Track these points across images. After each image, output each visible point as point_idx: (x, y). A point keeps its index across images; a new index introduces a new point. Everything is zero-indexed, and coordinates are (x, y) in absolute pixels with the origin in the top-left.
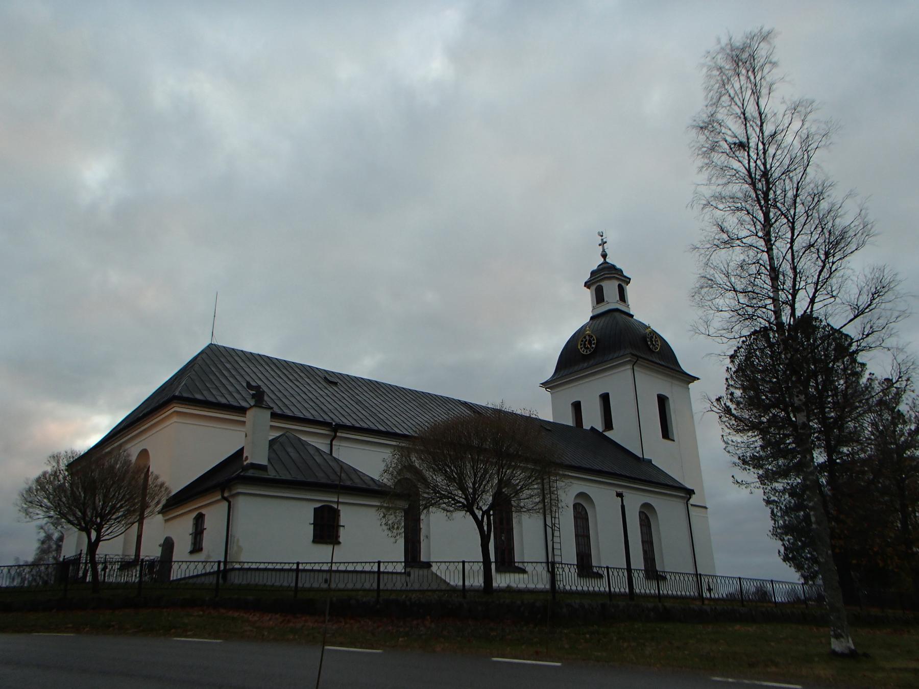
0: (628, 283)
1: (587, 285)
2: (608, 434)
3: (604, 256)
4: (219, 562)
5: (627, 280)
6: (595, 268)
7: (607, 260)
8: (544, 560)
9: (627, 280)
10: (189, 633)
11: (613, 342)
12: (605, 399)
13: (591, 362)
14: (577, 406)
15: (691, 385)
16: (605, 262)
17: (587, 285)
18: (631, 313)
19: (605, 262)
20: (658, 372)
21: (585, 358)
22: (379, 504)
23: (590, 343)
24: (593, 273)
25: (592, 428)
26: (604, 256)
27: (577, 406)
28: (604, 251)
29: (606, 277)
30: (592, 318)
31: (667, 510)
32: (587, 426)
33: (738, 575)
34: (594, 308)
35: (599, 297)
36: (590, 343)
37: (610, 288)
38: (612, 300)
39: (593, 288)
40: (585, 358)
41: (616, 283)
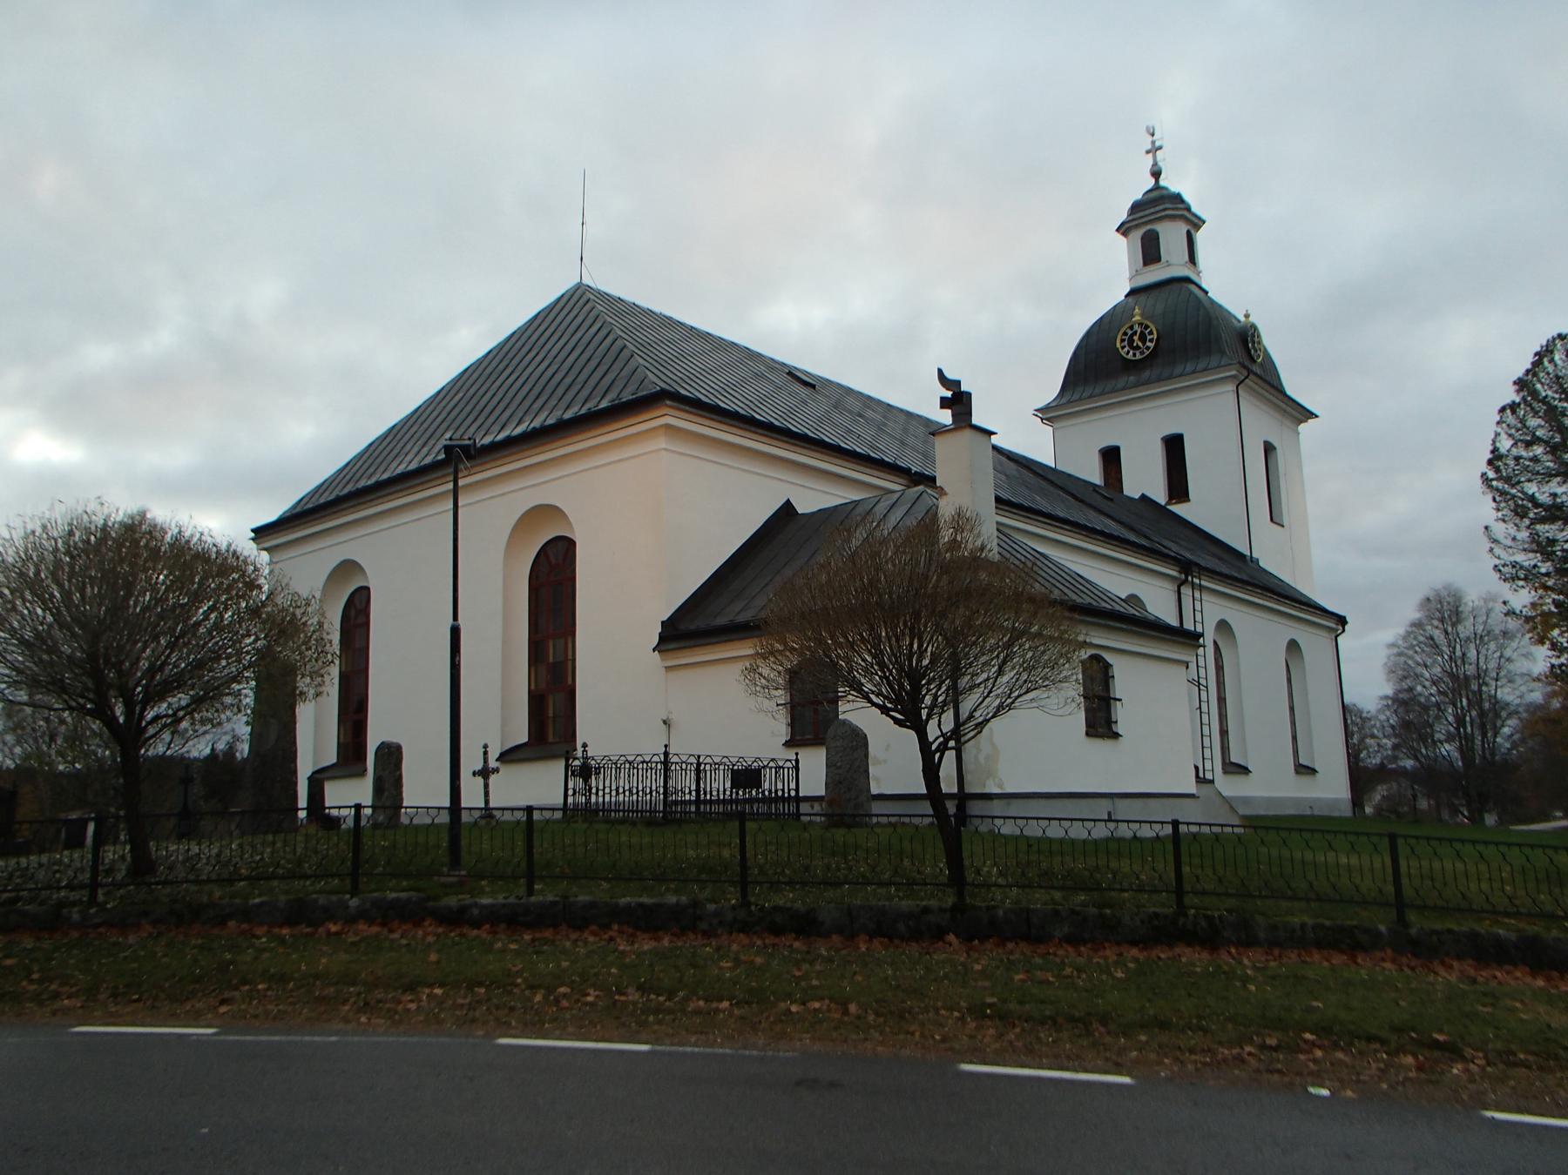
1: (1124, 229)
2: (1177, 509)
3: (1156, 174)
4: (358, 807)
5: (1196, 223)
6: (1139, 196)
7: (1162, 183)
9: (1196, 223)
11: (1166, 338)
12: (1174, 447)
13: (1147, 374)
14: (1111, 457)
15: (1302, 427)
16: (1157, 187)
17: (1124, 229)
19: (1157, 187)
21: (1129, 366)
22: (751, 652)
23: (1143, 338)
24: (1136, 207)
25: (1143, 497)
26: (1156, 174)
27: (1111, 457)
28: (1155, 164)
29: (1157, 215)
30: (1133, 293)
31: (1313, 642)
32: (1132, 489)
33: (523, 803)
34: (1135, 275)
35: (1151, 252)
36: (1143, 338)
37: (1171, 236)
38: (1173, 264)
39: (1137, 235)
40: (1129, 366)
41: (1183, 228)
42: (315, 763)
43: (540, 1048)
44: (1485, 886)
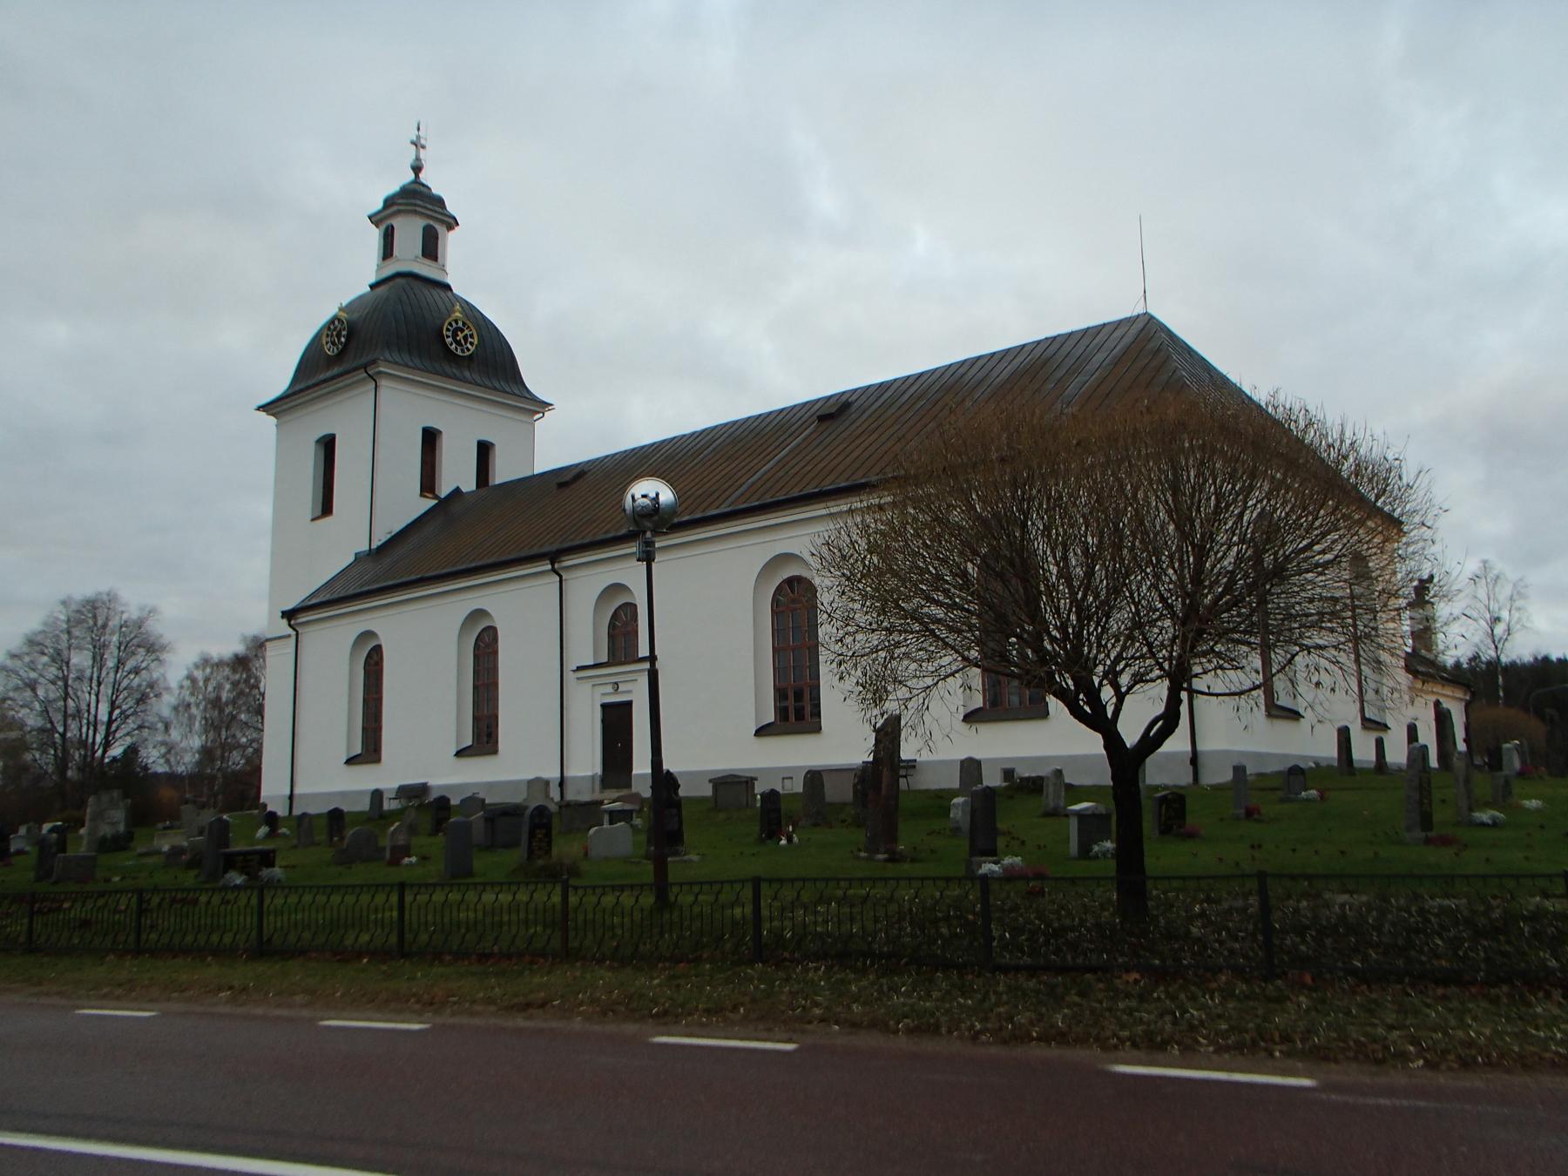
0: (450, 228)
1: (375, 219)
3: (417, 169)
8: (1200, 701)
9: (451, 223)
10: (298, 998)
16: (417, 181)
17: (375, 219)
18: (449, 281)
19: (417, 181)
20: (339, 398)
26: (417, 169)
28: (418, 159)
29: (417, 209)
34: (379, 268)
36: (339, 336)
38: (409, 257)
39: (383, 227)
40: (450, 356)
42: (458, 742)
43: (683, 1047)
44: (471, 915)
